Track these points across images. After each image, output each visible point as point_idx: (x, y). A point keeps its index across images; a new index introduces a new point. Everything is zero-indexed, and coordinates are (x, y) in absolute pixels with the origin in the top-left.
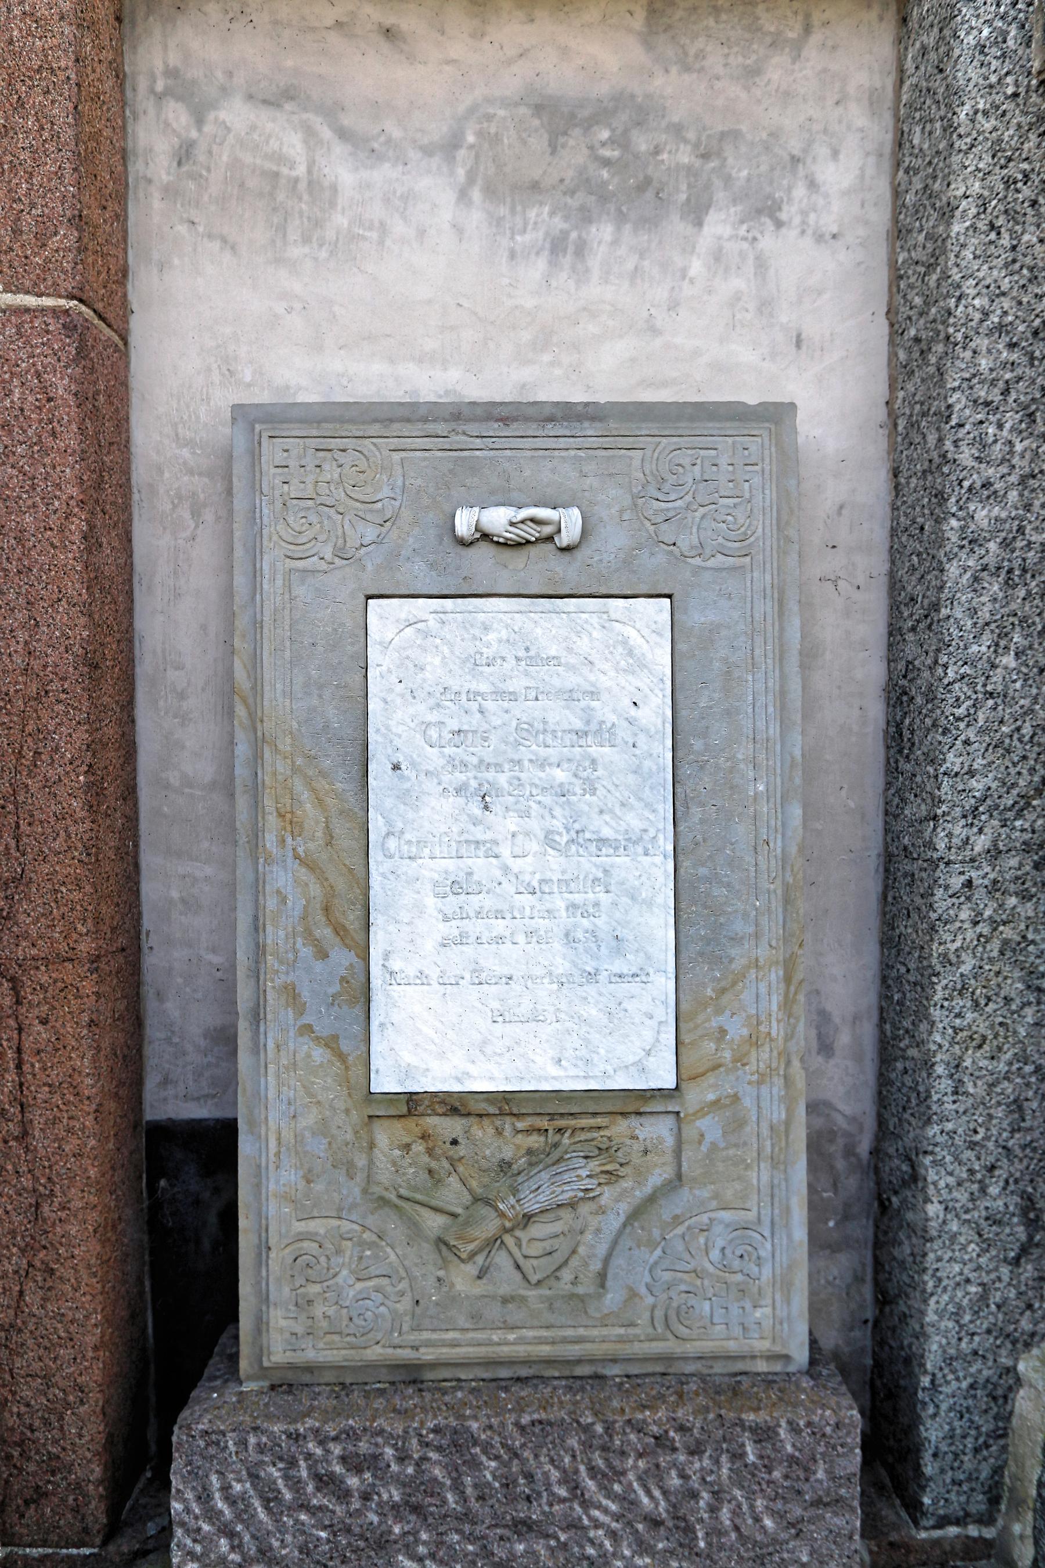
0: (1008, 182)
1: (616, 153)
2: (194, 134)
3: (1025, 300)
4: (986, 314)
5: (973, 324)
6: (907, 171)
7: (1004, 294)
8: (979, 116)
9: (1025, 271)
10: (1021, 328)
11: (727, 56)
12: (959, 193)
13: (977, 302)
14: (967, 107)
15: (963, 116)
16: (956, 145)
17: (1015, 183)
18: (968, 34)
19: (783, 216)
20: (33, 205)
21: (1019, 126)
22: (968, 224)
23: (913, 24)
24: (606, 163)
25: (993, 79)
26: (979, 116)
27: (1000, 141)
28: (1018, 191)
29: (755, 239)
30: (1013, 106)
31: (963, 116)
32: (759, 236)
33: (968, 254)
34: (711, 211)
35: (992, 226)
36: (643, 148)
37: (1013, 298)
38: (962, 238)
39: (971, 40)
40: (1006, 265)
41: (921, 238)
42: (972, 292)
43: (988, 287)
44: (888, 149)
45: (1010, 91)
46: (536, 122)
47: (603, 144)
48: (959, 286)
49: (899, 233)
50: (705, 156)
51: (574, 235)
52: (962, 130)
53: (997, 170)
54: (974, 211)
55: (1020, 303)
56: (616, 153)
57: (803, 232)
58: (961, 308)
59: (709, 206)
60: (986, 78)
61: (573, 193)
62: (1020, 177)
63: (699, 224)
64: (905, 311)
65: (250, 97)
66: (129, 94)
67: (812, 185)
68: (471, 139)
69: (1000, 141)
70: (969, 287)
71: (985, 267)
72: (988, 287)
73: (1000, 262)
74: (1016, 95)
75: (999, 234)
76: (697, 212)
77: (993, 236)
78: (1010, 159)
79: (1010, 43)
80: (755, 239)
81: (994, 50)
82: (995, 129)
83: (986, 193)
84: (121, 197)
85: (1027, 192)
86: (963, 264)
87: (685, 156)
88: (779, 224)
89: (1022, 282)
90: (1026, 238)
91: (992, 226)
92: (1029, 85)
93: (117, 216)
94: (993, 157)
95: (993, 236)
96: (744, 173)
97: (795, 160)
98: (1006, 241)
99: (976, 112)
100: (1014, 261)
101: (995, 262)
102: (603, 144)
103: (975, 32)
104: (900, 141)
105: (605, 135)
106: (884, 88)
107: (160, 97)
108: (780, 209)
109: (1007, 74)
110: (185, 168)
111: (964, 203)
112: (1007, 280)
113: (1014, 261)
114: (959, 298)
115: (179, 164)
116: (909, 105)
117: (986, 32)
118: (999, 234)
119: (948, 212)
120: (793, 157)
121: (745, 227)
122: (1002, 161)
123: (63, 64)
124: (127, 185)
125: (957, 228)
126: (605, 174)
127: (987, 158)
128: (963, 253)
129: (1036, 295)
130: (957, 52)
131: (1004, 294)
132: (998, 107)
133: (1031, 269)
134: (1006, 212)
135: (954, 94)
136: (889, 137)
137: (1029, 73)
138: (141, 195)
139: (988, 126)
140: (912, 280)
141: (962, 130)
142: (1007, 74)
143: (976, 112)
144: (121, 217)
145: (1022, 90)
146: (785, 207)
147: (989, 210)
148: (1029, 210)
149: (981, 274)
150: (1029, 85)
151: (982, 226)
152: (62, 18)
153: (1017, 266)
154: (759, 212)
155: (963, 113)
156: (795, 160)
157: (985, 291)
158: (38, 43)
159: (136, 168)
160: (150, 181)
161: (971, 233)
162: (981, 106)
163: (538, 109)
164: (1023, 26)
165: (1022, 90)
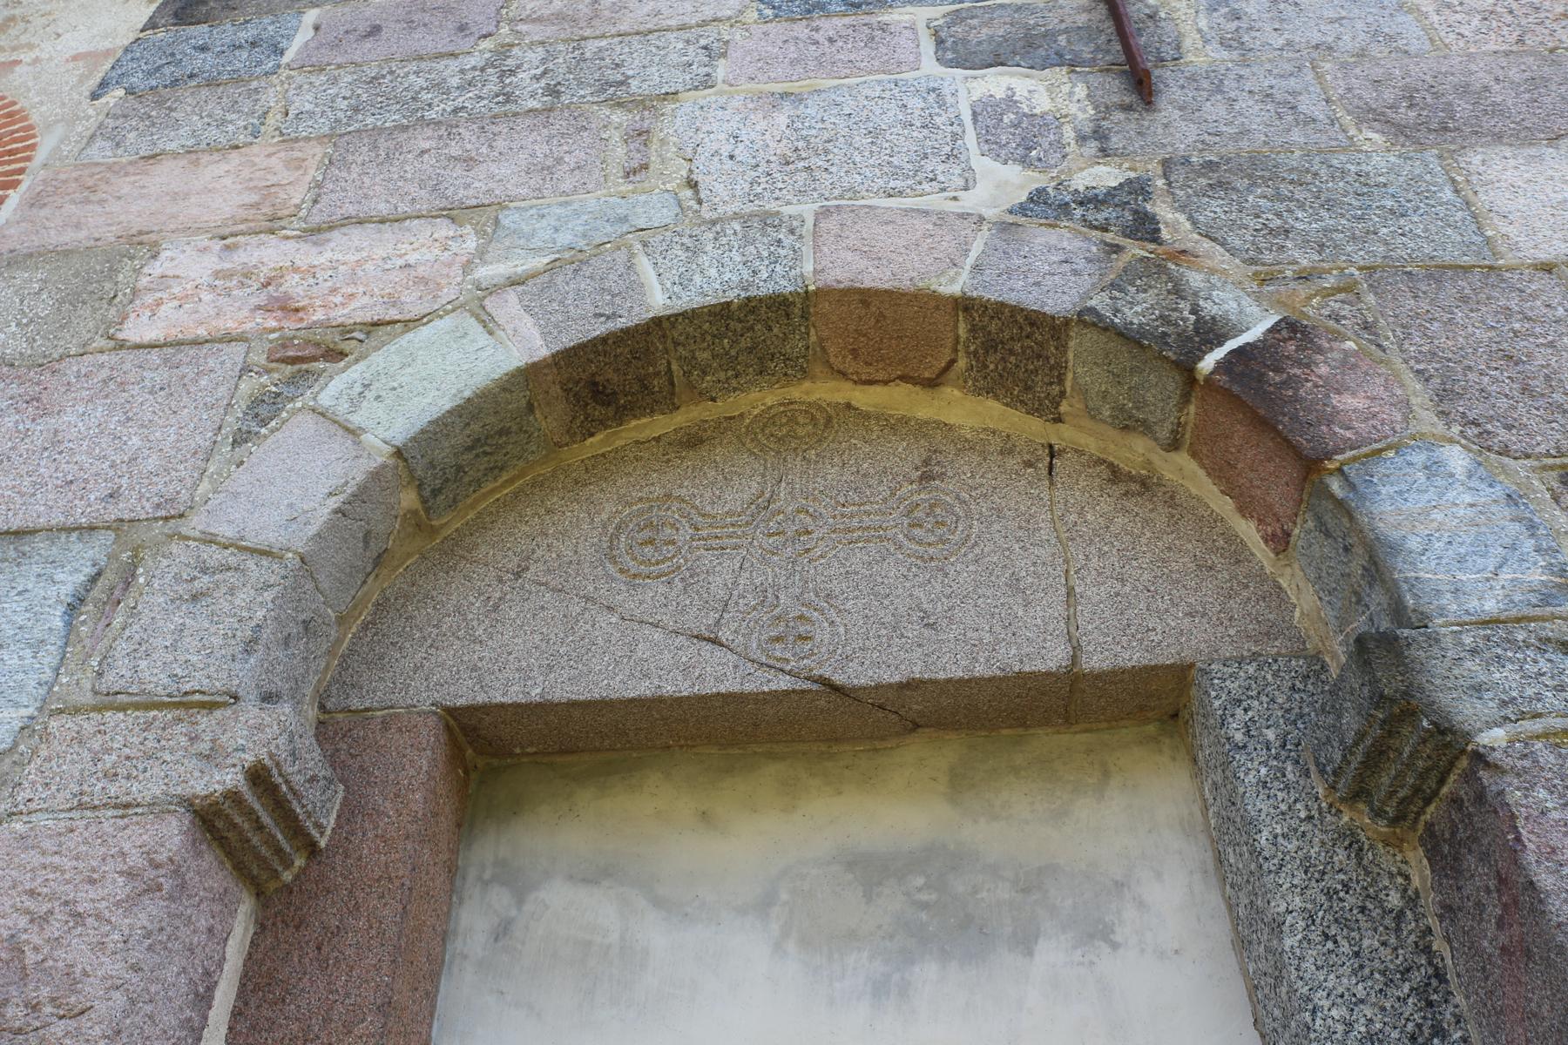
0: (1329, 894)
1: (934, 897)
2: (513, 913)
3: (1388, 1005)
4: (1349, 1025)
5: (1338, 1036)
6: (1232, 887)
7: (1362, 1001)
8: (1280, 840)
9: (1377, 976)
10: (1395, 1034)
11: (1032, 803)
12: (1282, 909)
13: (1334, 1013)
14: (1265, 833)
15: (1263, 841)
16: (1265, 866)
17: (1336, 892)
18: (1246, 774)
19: (1118, 938)
20: (348, 995)
21: (1323, 843)
22: (1299, 937)
23: (1201, 763)
24: (925, 906)
25: (1283, 807)
26: (1280, 840)
27: (1308, 858)
28: (1341, 900)
29: (1092, 963)
30: (1310, 827)
31: (1263, 841)
32: (1095, 959)
33: (1308, 965)
34: (1041, 941)
35: (1326, 937)
36: (961, 889)
37: (1374, 1005)
38: (1298, 951)
39: (1251, 778)
40: (1354, 972)
41: (1262, 949)
42: (1326, 1003)
43: (1342, 996)
44: (1211, 865)
45: (1303, 815)
46: (850, 876)
47: (920, 890)
48: (1309, 999)
49: (1242, 944)
50: (1026, 891)
51: (896, 977)
52: (1266, 854)
53: (1313, 883)
54: (1302, 924)
55: (1383, 1009)
56: (934, 897)
57: (1143, 951)
58: (1319, 1022)
59: (1037, 937)
60: (1276, 808)
61: (892, 937)
62: (1339, 887)
63: (1030, 953)
64: (1269, 1024)
65: (571, 877)
66: (458, 883)
67: (1141, 905)
68: (784, 896)
69: (1308, 858)
70: (1320, 998)
71: (1332, 976)
72: (1342, 996)
73: (1347, 970)
74: (1310, 818)
75: (1336, 942)
76: (1025, 942)
77: (1330, 945)
78: (1324, 873)
79: (1290, 776)
80: (1092, 963)
81: (1276, 784)
82: (1300, 848)
83: (1309, 906)
84: (434, 977)
85: (1351, 900)
86: (1307, 976)
87: (1004, 892)
88: (1115, 946)
89: (1377, 988)
90: (1366, 943)
91: (1326, 937)
92: (1320, 808)
93: (427, 994)
94: (1306, 873)
95: (1330, 945)
96: (1069, 902)
97: (1119, 885)
98: (1345, 947)
99: (1276, 837)
100: (1362, 967)
101: (1341, 971)
102: (920, 890)
103: (1254, 772)
104: (1220, 860)
105: (920, 881)
106: (1191, 814)
107: (486, 884)
108: (1113, 932)
109: (1296, 801)
110: (500, 944)
111: (1289, 918)
112: (1360, 987)
113: (1362, 967)
114: (1314, 1012)
115: (496, 940)
116: (1218, 828)
117: (1263, 771)
118: (1336, 942)
119: (1277, 927)
120: (1116, 883)
121: (1079, 952)
122: (1317, 875)
123: (400, 873)
124: (443, 961)
125: (1288, 942)
126: (924, 916)
127: (1300, 874)
128: (1304, 965)
129: (1399, 999)
130: (1241, 790)
131: (1362, 1001)
132: (1296, 830)
133: (1383, 973)
134: (1336, 920)
135: (1250, 826)
136: (1210, 854)
137: (1317, 799)
138: (455, 970)
139: (1291, 847)
140: (1267, 991)
141: (1266, 854)
142: (1296, 801)
143: (1276, 837)
144: (431, 996)
145: (1315, 813)
146: (1117, 929)
147: (1318, 921)
148: (1360, 916)
149: (1330, 985)
150: (1320, 808)
151: (1315, 937)
152: (407, 838)
153: (1367, 971)
154: (1091, 936)
155: (1263, 838)
156: (1119, 885)
157: (1339, 1000)
158: (383, 858)
159: (457, 945)
160: (465, 957)
161: (1305, 944)
162: (1279, 831)
163: (850, 865)
164: (1297, 762)
165: (1315, 813)
